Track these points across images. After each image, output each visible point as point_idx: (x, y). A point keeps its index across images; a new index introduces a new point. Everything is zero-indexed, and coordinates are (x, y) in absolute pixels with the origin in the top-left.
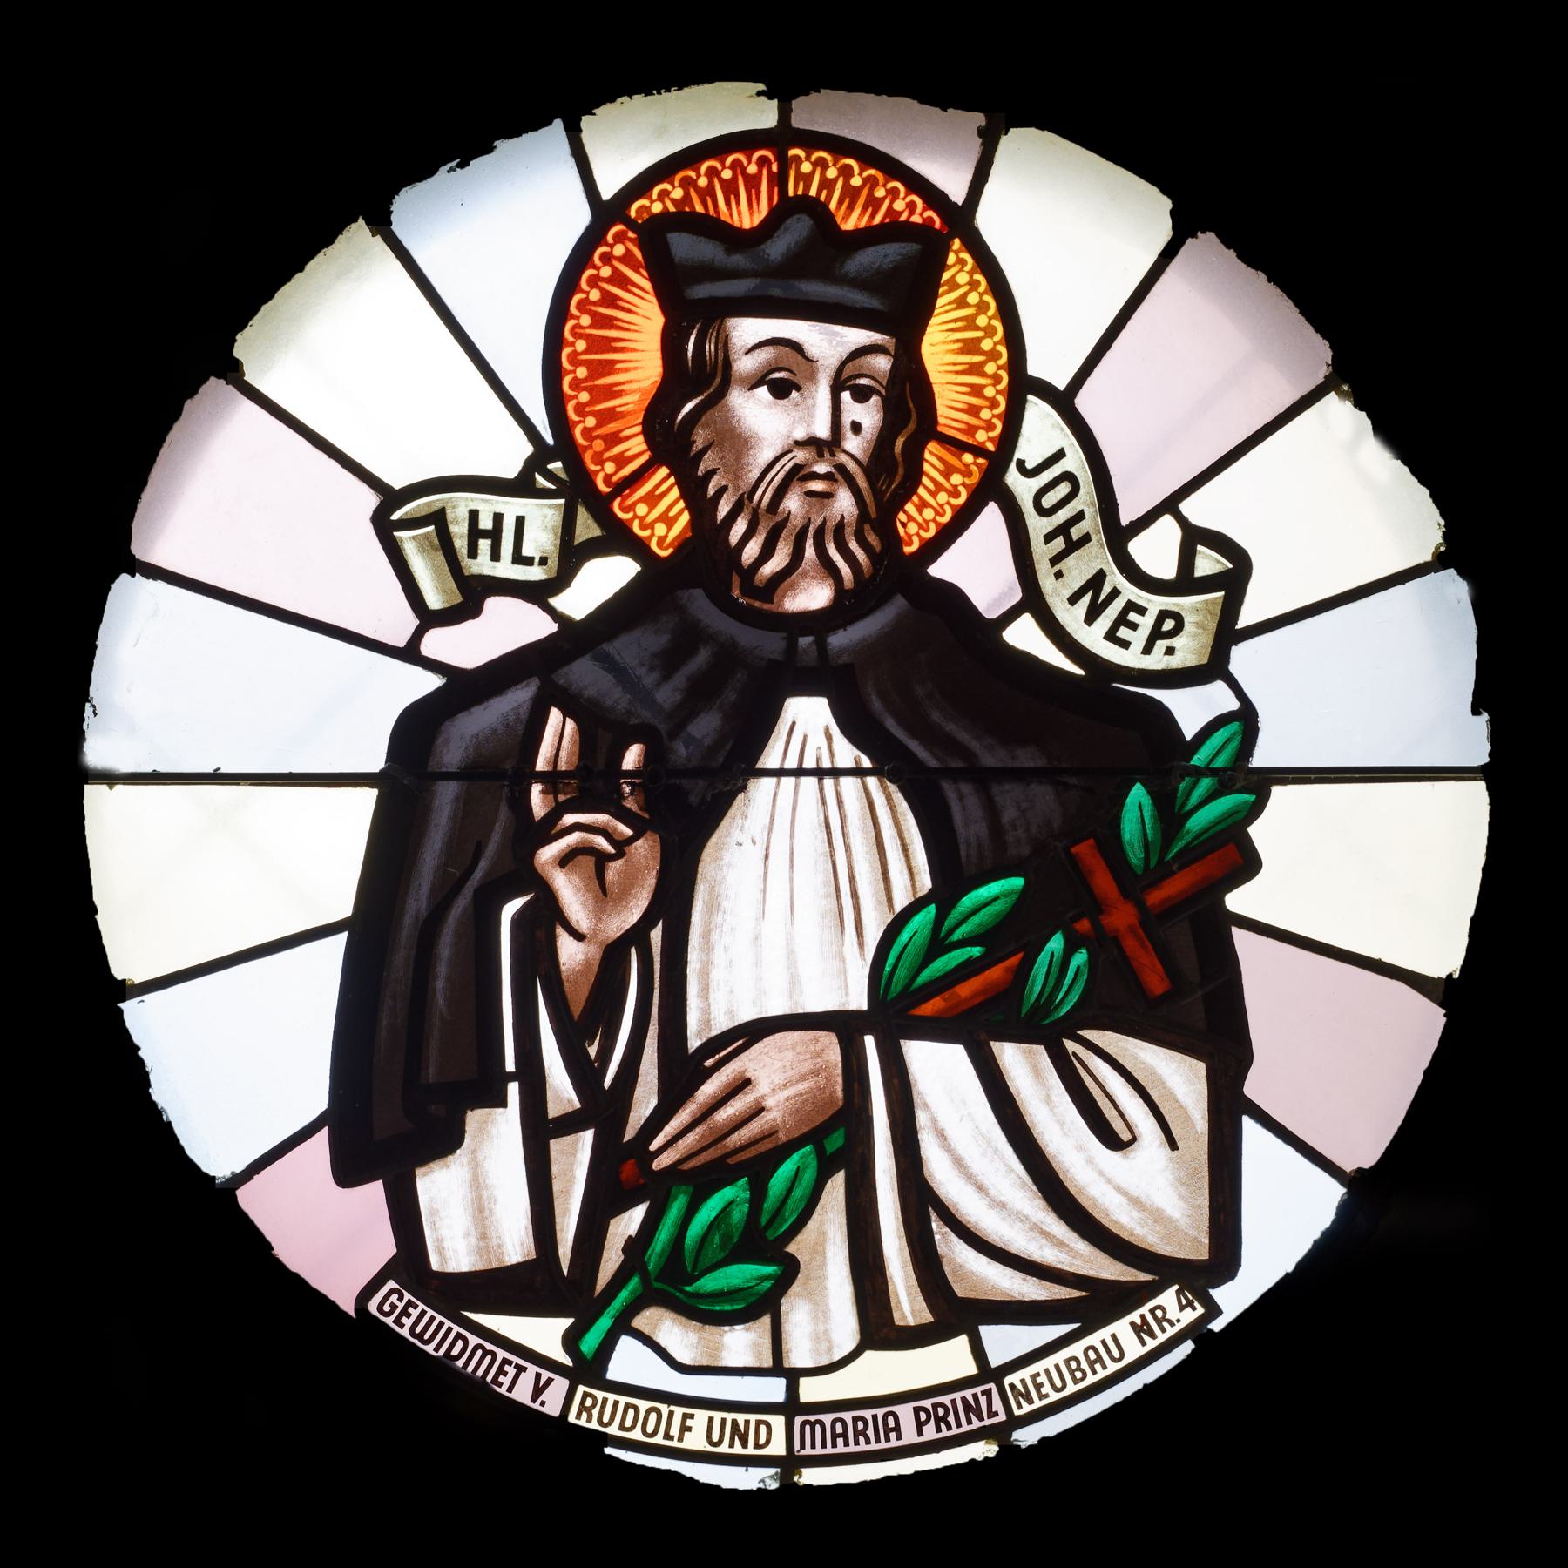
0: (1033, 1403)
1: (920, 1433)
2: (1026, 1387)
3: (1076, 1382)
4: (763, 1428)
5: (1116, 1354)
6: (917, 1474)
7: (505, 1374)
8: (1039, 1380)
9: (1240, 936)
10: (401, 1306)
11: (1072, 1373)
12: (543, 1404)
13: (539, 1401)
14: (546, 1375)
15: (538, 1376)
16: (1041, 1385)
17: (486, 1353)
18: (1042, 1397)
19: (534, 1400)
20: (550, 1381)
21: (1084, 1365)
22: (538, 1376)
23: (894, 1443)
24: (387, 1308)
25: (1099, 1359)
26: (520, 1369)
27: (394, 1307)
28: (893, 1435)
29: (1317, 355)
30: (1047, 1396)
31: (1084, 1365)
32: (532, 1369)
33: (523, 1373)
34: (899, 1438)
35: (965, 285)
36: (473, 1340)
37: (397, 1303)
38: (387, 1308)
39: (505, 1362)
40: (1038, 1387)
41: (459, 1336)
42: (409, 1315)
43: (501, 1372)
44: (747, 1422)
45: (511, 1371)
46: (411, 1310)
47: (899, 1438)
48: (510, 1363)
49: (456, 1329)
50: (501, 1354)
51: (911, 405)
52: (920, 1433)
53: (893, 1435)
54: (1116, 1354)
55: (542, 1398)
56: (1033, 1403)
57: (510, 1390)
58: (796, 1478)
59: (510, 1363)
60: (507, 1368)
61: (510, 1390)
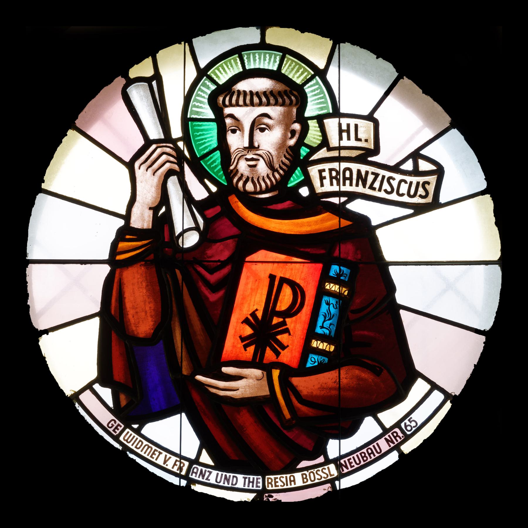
0: (225, 475)
1: (173, 468)
2: (200, 475)
3: (364, 461)
4: (235, 479)
5: (379, 451)
6: (90, 425)
7: (155, 455)
8: (351, 461)
9: (402, 312)
10: (115, 425)
11: (363, 458)
12: (167, 465)
13: (166, 464)
14: (169, 455)
15: (166, 456)
16: (352, 463)
17: (149, 447)
18: (352, 467)
19: (164, 463)
20: (170, 458)
21: (367, 455)
22: (166, 456)
23: (293, 486)
24: (110, 425)
25: (372, 453)
26: (160, 453)
27: (113, 425)
28: (293, 483)
29: (447, 120)
30: (354, 466)
31: (367, 455)
32: (164, 453)
33: (161, 455)
34: (295, 484)
35: (252, 378)
36: (145, 443)
37: (114, 424)
38: (110, 425)
39: (155, 450)
40: (350, 463)
41: (140, 441)
42: (118, 429)
43: (154, 453)
44: (230, 476)
45: (157, 453)
46: (119, 427)
47: (295, 484)
48: (157, 451)
49: (139, 438)
50: (154, 448)
51: (271, 305)
52: (173, 468)
53: (293, 483)
54: (379, 451)
55: (167, 463)
56: (225, 475)
57: (156, 459)
58: (26, 258)
59: (157, 451)
60: (156, 452)
61: (156, 459)
